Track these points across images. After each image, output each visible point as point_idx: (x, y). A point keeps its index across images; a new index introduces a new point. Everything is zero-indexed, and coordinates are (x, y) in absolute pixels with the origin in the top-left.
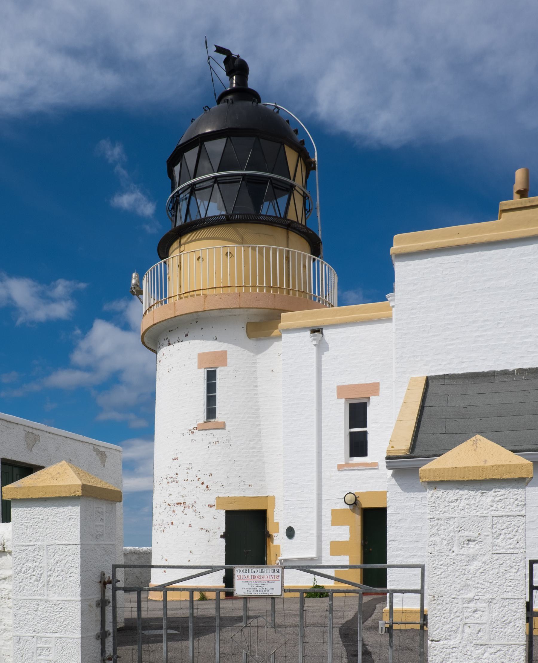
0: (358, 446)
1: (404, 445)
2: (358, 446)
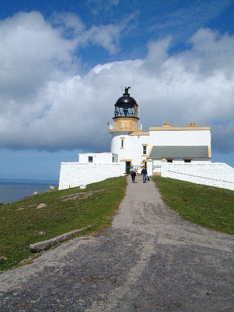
0: (145, 153)
1: (129, 92)
2: (145, 153)
